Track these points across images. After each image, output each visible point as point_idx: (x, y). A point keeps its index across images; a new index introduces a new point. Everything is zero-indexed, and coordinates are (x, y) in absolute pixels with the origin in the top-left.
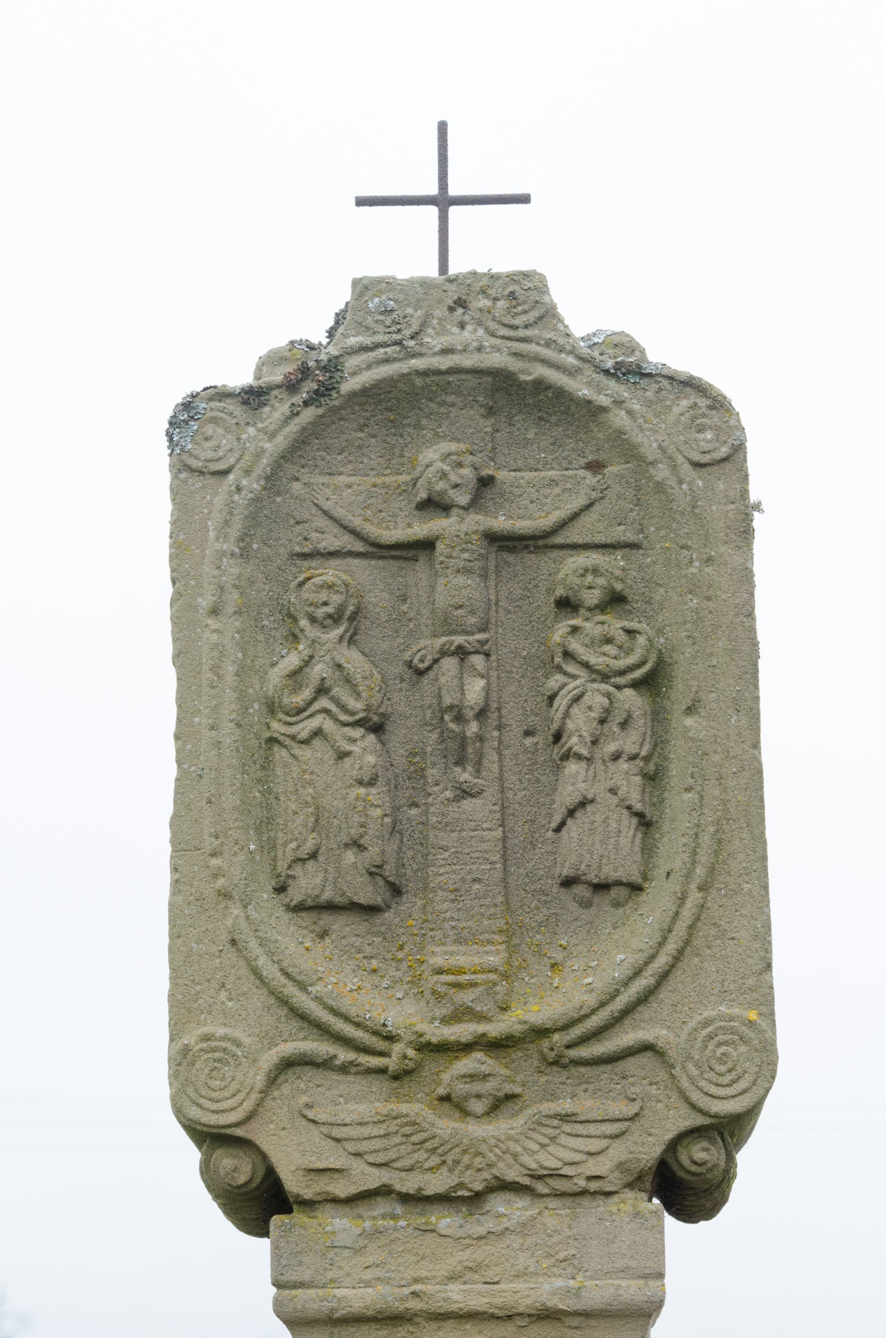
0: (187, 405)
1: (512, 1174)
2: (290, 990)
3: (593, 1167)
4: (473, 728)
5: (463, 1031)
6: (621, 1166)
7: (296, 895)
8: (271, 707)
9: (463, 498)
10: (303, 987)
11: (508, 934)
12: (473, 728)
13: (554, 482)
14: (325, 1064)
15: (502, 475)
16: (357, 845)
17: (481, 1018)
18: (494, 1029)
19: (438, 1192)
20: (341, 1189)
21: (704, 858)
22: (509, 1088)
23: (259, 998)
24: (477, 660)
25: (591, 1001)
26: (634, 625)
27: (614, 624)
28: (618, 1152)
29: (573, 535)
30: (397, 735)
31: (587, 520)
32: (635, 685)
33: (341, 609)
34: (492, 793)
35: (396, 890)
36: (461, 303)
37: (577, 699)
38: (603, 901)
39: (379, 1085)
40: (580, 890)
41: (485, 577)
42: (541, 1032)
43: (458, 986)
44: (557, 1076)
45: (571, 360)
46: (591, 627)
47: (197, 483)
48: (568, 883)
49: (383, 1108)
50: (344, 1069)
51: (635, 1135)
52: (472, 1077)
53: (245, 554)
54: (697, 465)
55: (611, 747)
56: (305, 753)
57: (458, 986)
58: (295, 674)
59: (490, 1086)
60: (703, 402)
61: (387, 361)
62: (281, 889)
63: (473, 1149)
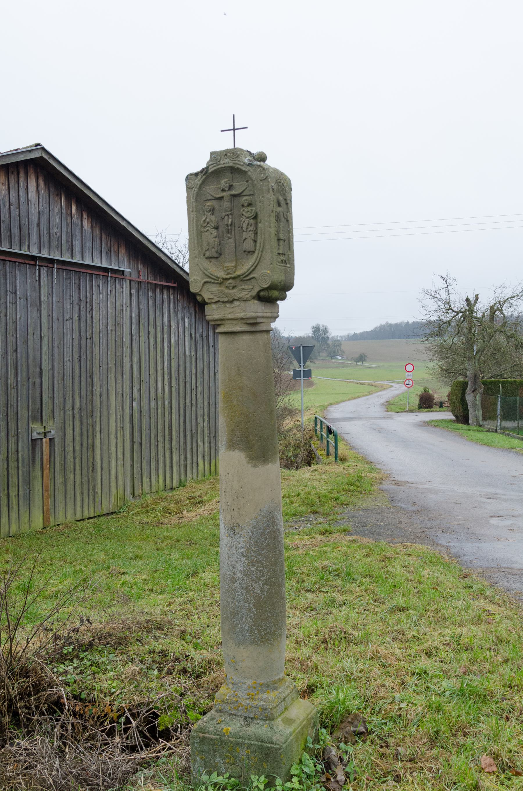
0: (187, 177)
1: (236, 298)
2: (205, 271)
3: (247, 296)
4: (230, 228)
5: (228, 276)
6: (251, 296)
7: (206, 256)
8: (202, 226)
9: (227, 189)
10: (206, 271)
11: (236, 260)
12: (230, 228)
13: (241, 185)
14: (210, 282)
15: (234, 184)
16: (213, 248)
17: (231, 274)
18: (232, 276)
19: (416, 320)
20: (213, 301)
21: (261, 247)
22: (235, 285)
23: (201, 273)
24: (230, 216)
25: (246, 271)
26: (252, 208)
27: (250, 209)
28: (250, 294)
29: (244, 194)
30: (221, 229)
31: (246, 191)
32: (253, 219)
33: (210, 209)
34: (233, 238)
35: (220, 254)
36: (226, 155)
37: (244, 222)
38: (250, 254)
39: (218, 285)
40: (246, 253)
41: (231, 202)
42: (239, 276)
43: (228, 269)
44: (242, 283)
45: (242, 163)
46: (246, 210)
47: (189, 190)
48: (245, 251)
49: (218, 288)
50: (213, 283)
51: (253, 291)
52: (230, 283)
53: (196, 201)
54: (261, 180)
55: (249, 229)
56: (206, 233)
57: (228, 269)
58: (204, 221)
59: (232, 285)
60: (262, 169)
61: (215, 166)
62: (204, 255)
63: (230, 294)
